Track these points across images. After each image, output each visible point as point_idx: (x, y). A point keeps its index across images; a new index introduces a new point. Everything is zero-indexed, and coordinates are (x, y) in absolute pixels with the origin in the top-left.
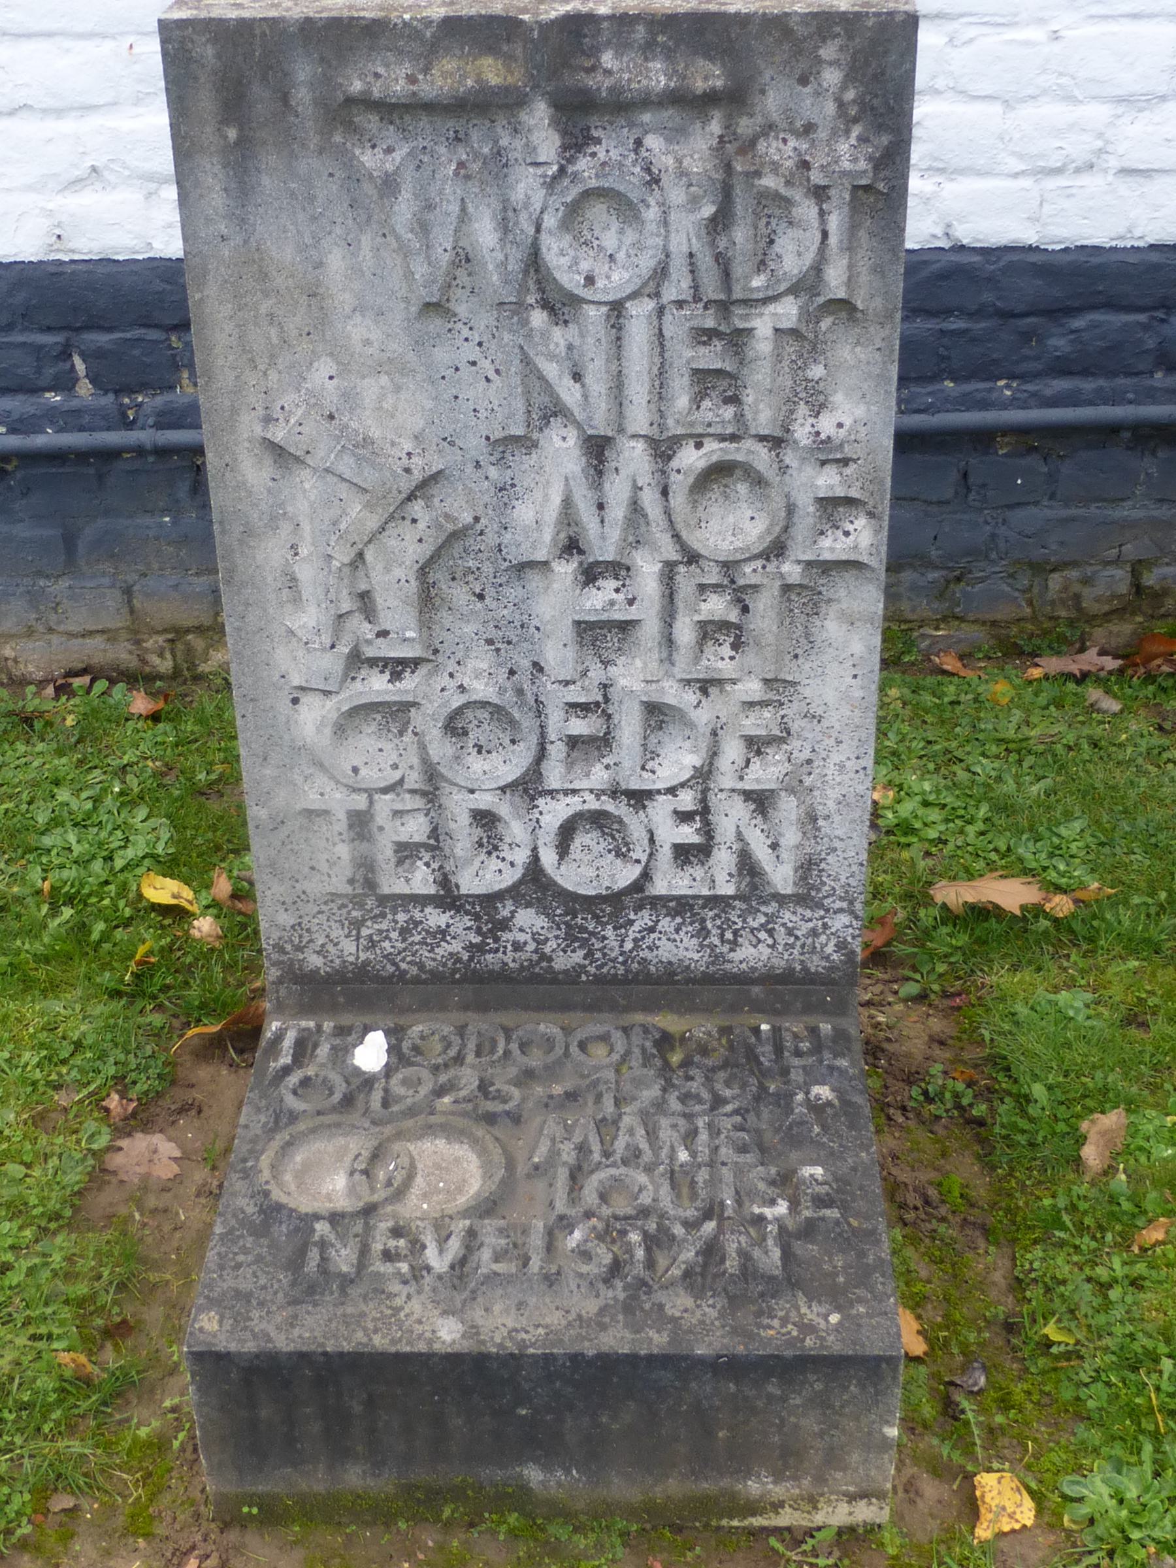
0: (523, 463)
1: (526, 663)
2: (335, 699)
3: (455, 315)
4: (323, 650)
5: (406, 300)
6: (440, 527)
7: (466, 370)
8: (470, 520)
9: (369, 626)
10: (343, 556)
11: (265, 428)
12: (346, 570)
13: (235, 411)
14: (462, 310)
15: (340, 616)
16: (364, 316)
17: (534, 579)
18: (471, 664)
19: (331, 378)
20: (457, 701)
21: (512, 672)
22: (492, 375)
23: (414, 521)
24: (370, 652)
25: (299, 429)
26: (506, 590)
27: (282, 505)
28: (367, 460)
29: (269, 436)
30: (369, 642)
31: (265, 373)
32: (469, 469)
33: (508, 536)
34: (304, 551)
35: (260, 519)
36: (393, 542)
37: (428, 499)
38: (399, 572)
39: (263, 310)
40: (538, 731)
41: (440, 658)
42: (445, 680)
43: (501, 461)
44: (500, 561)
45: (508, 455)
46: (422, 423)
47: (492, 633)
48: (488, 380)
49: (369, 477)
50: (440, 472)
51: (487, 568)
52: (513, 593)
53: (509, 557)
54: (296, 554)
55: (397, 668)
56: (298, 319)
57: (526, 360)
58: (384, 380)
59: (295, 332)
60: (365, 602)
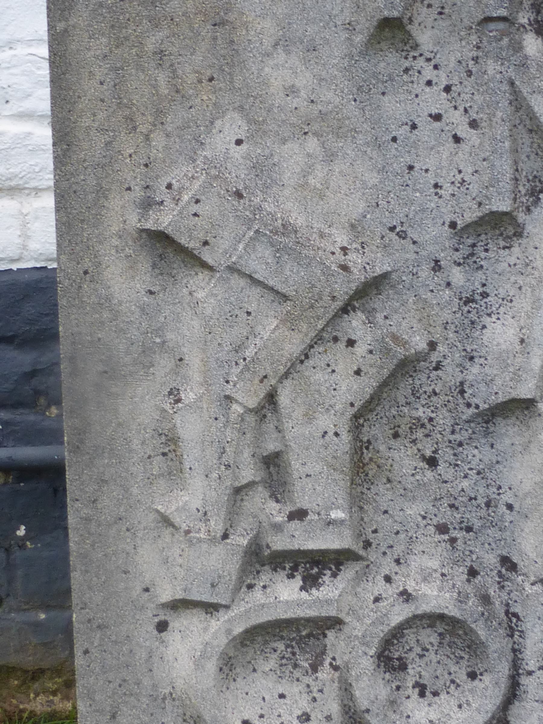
0: (501, 261)
1: (491, 559)
2: (224, 616)
3: (416, 46)
4: (212, 541)
5: (350, 27)
6: (387, 351)
7: (427, 130)
8: (422, 346)
9: (277, 506)
10: (249, 396)
11: (143, 216)
12: (251, 419)
13: (102, 193)
14: (425, 38)
15: (238, 490)
16: (288, 52)
17: (509, 433)
18: (416, 562)
19: (239, 142)
20: (399, 614)
21: (473, 573)
22: (463, 131)
23: (351, 343)
24: (279, 543)
25: (195, 208)
26: (468, 451)
27: (159, 331)
28: (286, 249)
29: (149, 225)
30: (277, 528)
31: (147, 138)
32: (425, 272)
33: (475, 369)
34: (189, 396)
35: (128, 352)
36: (319, 376)
37: (370, 313)
38: (325, 422)
39: (150, 46)
40: (510, 657)
41: (373, 555)
42: (379, 587)
43: (470, 261)
44: (462, 407)
45: (479, 249)
46: (362, 205)
47: (446, 515)
48: (457, 139)
49: (291, 277)
50: (385, 276)
51: (443, 419)
52: (477, 455)
53: (474, 401)
54: (178, 401)
55: (313, 566)
56: (198, 58)
57: (518, 102)
58: (312, 144)
59: (192, 78)
60: (273, 464)
